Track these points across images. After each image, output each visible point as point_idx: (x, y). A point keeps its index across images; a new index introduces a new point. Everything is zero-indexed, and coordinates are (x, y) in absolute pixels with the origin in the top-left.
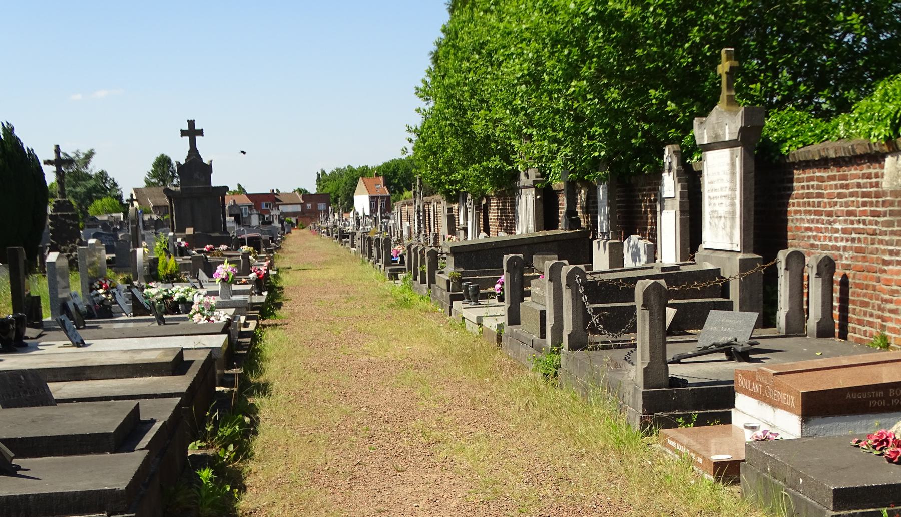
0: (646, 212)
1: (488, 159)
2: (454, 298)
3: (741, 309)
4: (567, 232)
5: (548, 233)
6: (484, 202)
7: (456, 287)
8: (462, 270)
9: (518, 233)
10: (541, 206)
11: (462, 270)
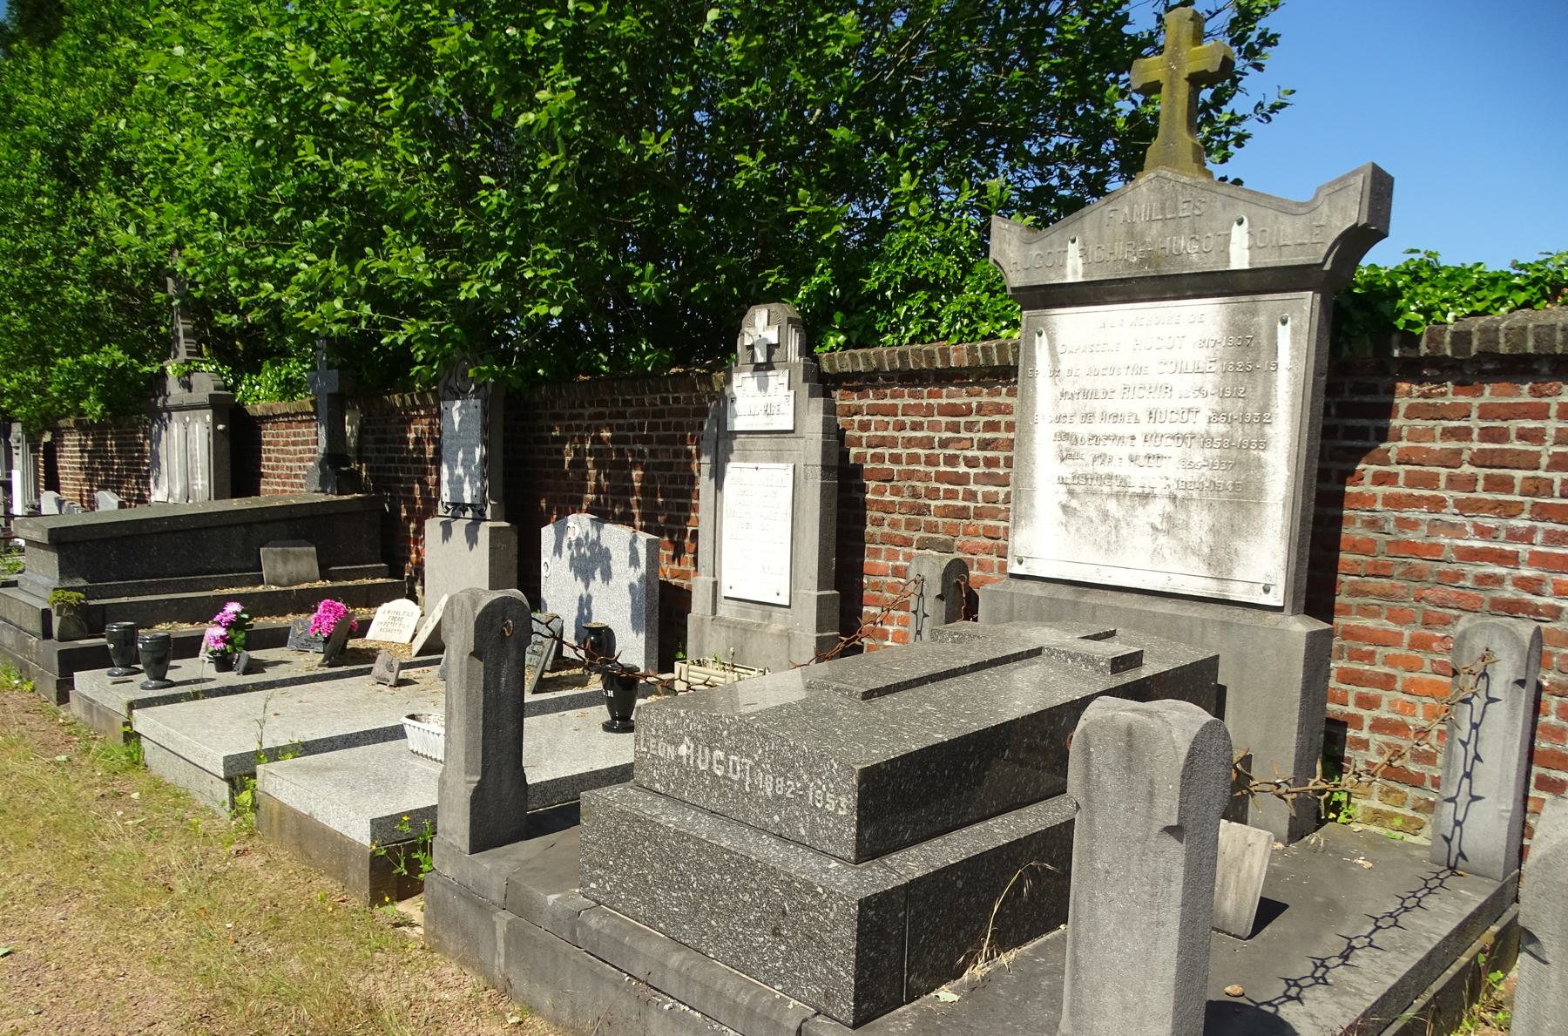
0: (578, 464)
1: (96, 348)
2: (71, 663)
3: (61, 653)
4: (335, 498)
5: (235, 504)
6: (47, 438)
7: (72, 628)
8: (82, 583)
9: (158, 495)
10: (226, 445)
11: (82, 583)
